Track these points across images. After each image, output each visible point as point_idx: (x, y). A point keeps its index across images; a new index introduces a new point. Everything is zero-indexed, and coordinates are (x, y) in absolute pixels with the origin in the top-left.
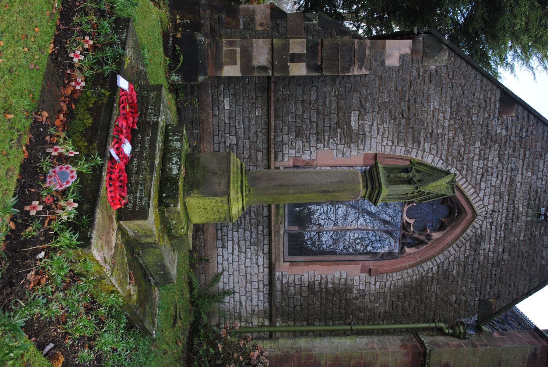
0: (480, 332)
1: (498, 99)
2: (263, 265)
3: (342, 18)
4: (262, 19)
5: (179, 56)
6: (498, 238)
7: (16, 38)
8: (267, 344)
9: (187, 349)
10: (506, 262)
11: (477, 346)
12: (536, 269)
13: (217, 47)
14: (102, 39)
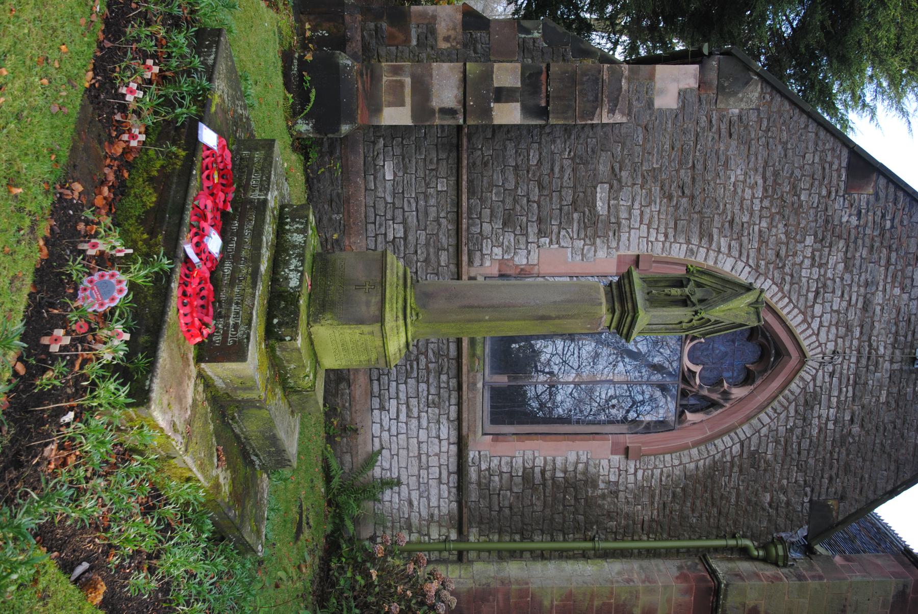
0: (813, 556)
1: (844, 164)
2: (448, 439)
3: (587, 27)
4: (448, 30)
5: (309, 91)
6: (843, 398)
7: (28, 62)
8: (453, 571)
9: (320, 578)
10: (857, 439)
11: (806, 579)
12: (907, 450)
13: (371, 77)
14: (174, 63)
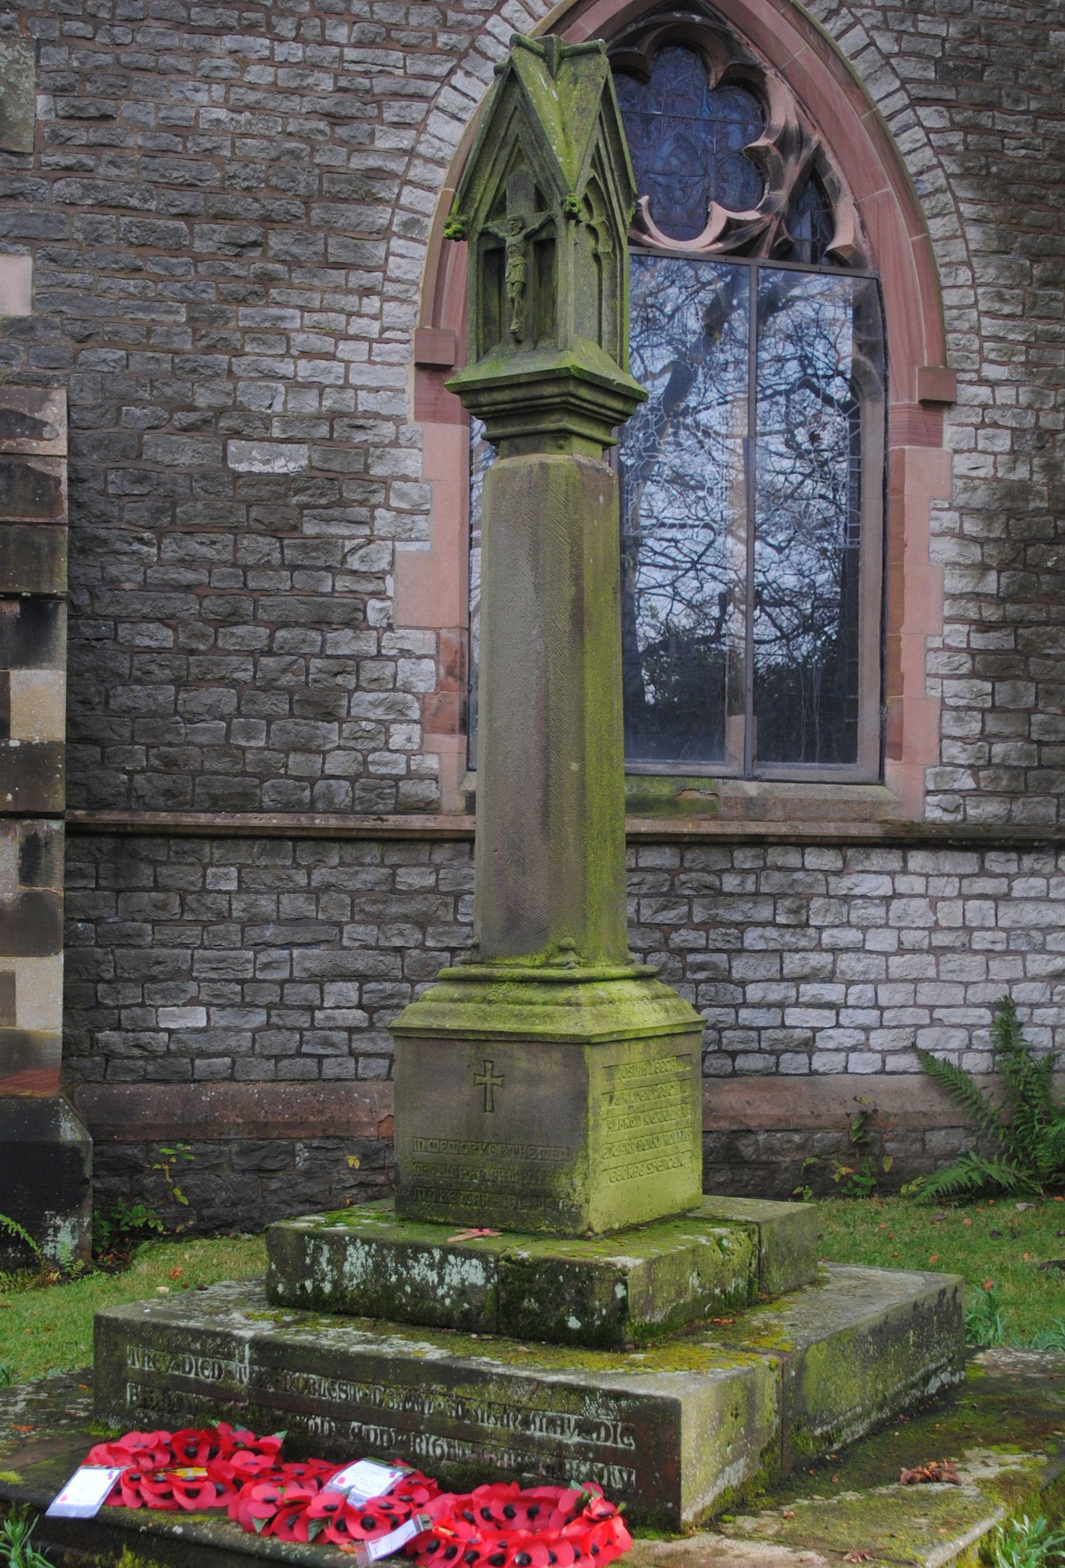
2: (892, 874)
